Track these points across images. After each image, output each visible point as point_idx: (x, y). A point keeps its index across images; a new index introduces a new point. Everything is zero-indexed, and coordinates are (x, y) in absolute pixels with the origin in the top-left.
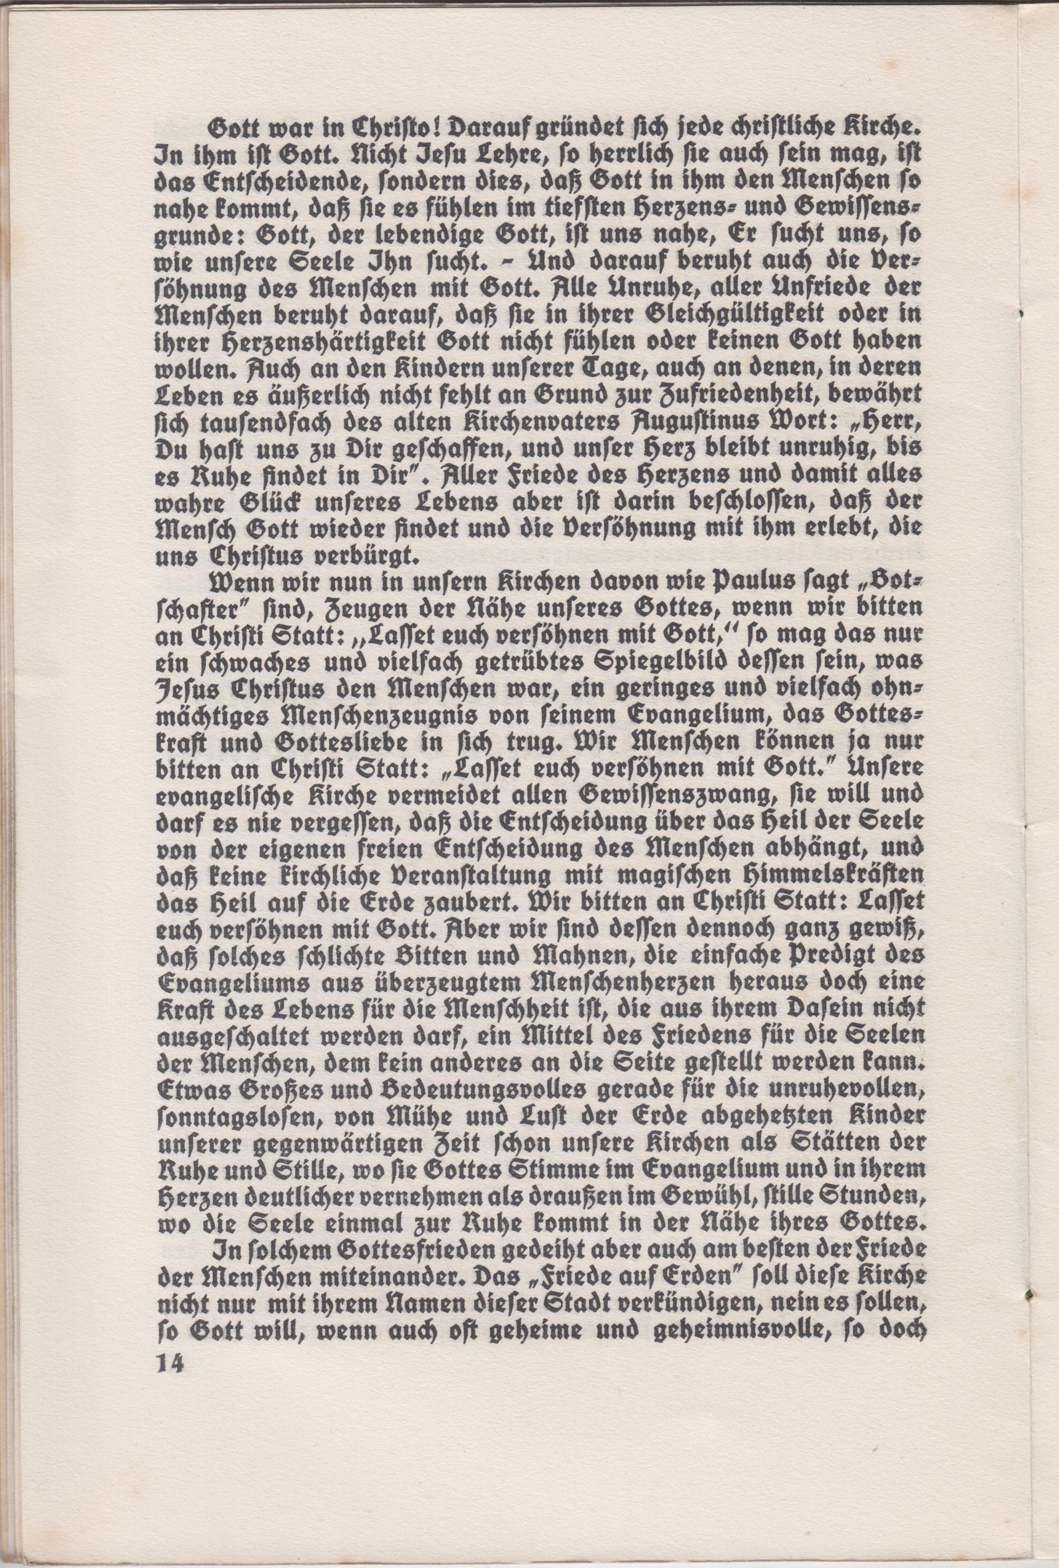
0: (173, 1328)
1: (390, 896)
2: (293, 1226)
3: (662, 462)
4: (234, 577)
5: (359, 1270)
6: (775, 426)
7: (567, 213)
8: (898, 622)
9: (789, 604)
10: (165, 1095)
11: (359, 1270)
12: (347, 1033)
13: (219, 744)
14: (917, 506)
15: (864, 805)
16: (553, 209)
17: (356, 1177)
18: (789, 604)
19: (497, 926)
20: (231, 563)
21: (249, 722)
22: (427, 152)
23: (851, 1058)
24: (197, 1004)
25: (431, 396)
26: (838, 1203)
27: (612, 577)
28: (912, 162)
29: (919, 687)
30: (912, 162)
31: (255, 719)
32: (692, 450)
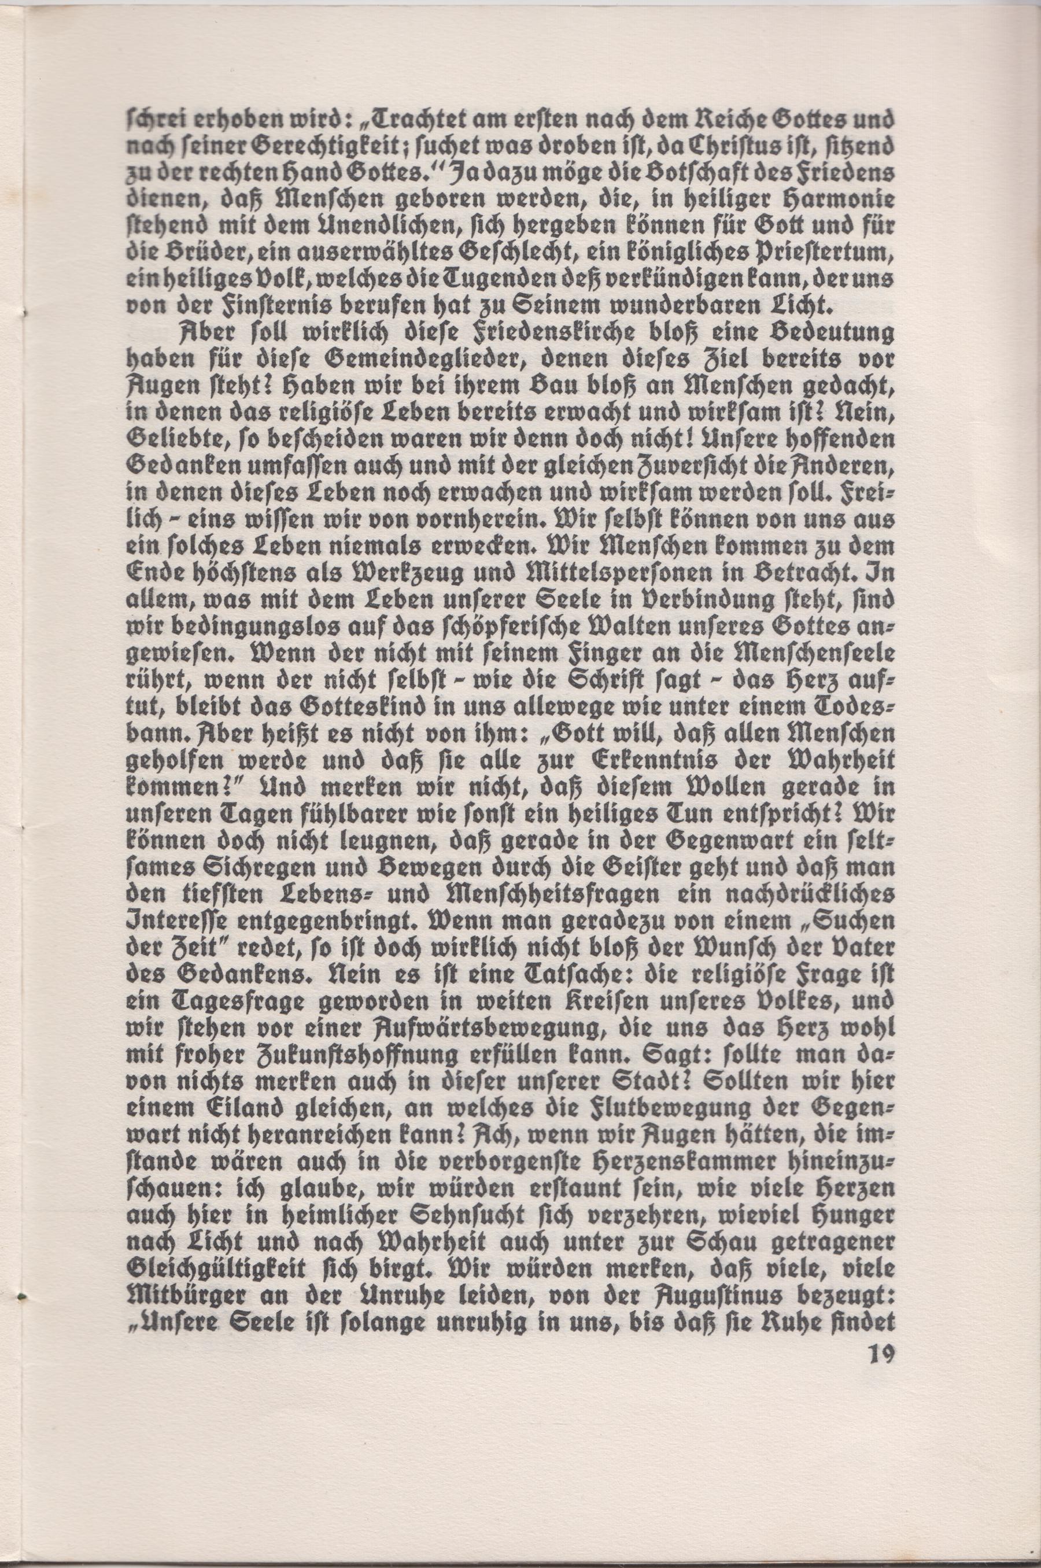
0: (326, 944)
3: (834, 1203)
4: (378, 567)
6: (593, 633)
7: (205, 900)
8: (152, 1095)
13: (463, 1003)
14: (890, 1248)
16: (191, 895)
17: (531, 1141)
22: (137, 917)
23: (704, 543)
25: (239, 1136)
26: (631, 1089)
27: (232, 970)
28: (449, 984)
30: (449, 984)
32: (825, 1031)
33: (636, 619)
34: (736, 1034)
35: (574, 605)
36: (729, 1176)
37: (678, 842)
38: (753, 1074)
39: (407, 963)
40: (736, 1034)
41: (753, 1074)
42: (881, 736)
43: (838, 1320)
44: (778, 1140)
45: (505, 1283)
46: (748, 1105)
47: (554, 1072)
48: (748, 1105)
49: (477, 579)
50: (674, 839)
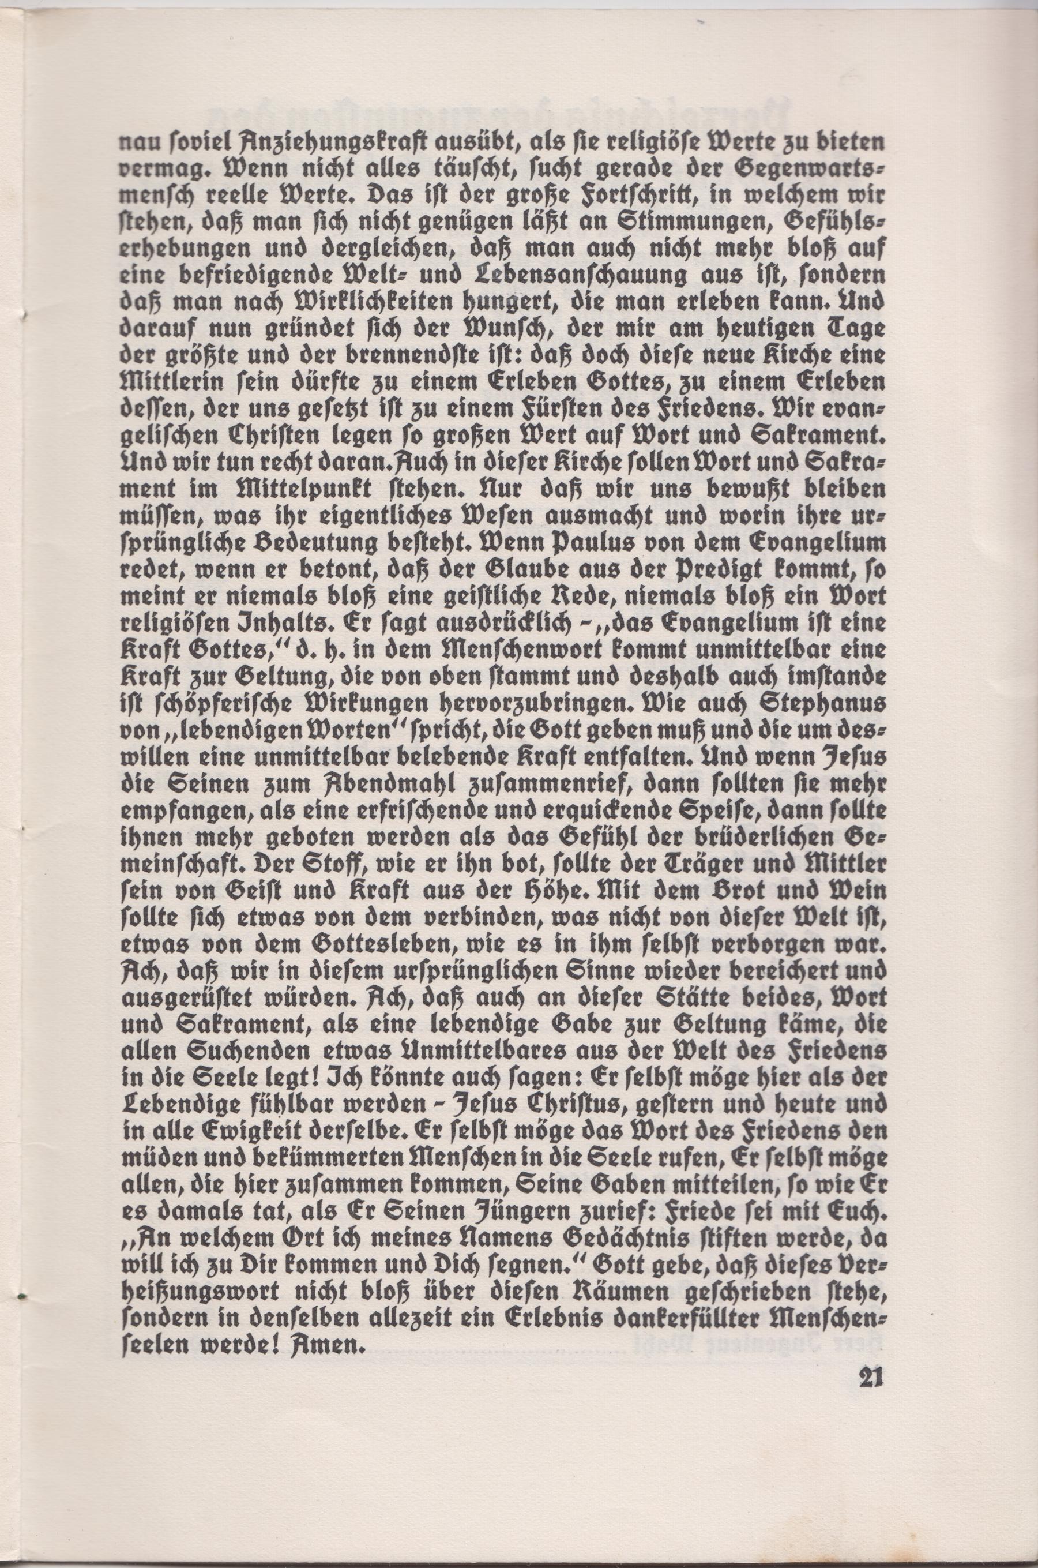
1: (311, 991)
2: (631, 1160)
5: (332, 750)
9: (248, 326)
10: (124, 280)
11: (332, 750)
12: (444, 913)
15: (570, 955)
18: (248, 326)
19: (741, 861)
20: (548, 1110)
21: (745, 227)
24: (742, 1259)
29: (882, 408)
31: (761, 1054)
33: (651, 750)
34: (133, 308)
35: (231, 1084)
36: (497, 931)
37: (599, 383)
38: (157, 911)
39: (529, 932)
40: (133, 308)
41: (157, 911)
42: (280, 947)
43: (301, 1342)
44: (652, 602)
45: (425, 933)
46: (763, 1022)
47: (761, 908)
48: (763, 1022)
49: (397, 977)
50: (595, 380)
